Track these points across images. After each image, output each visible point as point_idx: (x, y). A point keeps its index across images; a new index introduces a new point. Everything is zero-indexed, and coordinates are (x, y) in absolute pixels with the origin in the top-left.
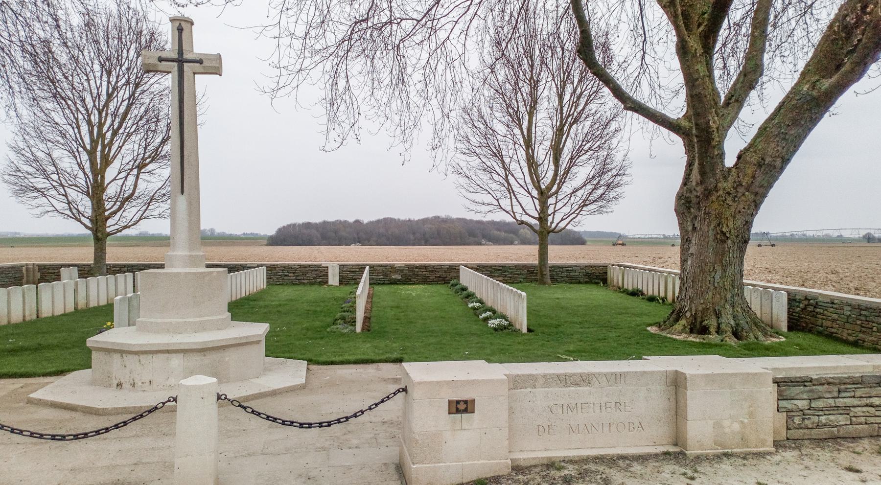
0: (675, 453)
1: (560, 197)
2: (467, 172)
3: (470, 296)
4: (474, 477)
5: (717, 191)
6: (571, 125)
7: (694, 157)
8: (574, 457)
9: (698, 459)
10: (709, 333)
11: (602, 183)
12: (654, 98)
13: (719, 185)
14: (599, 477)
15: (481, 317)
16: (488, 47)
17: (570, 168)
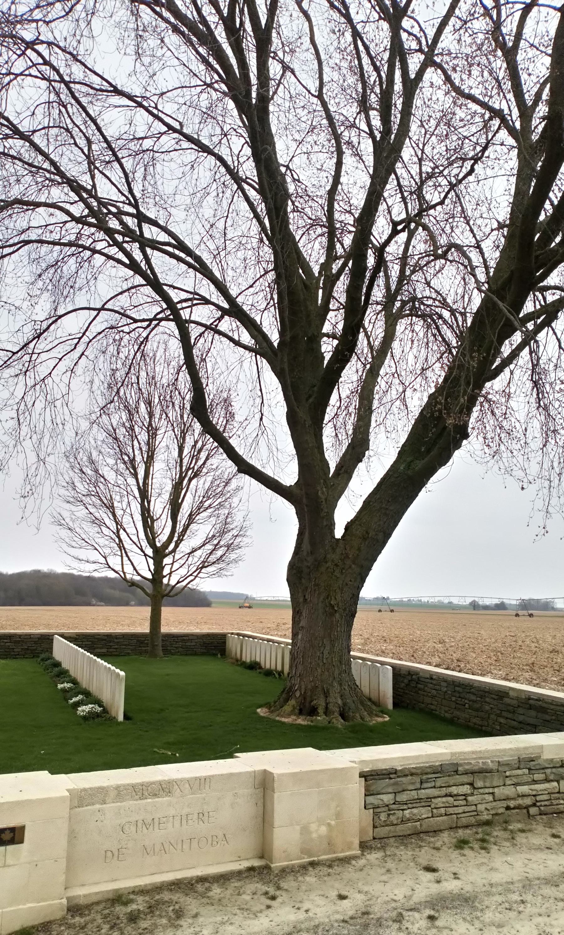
0: (260, 867)
1: (177, 557)
2: (71, 524)
3: (63, 674)
4: (16, 926)
5: (326, 562)
6: (190, 480)
7: (305, 526)
8: (146, 885)
9: (284, 872)
10: (317, 714)
11: (222, 543)
12: (272, 460)
13: (328, 556)
14: (171, 908)
15: (71, 701)
16: (100, 386)
17: (188, 525)
